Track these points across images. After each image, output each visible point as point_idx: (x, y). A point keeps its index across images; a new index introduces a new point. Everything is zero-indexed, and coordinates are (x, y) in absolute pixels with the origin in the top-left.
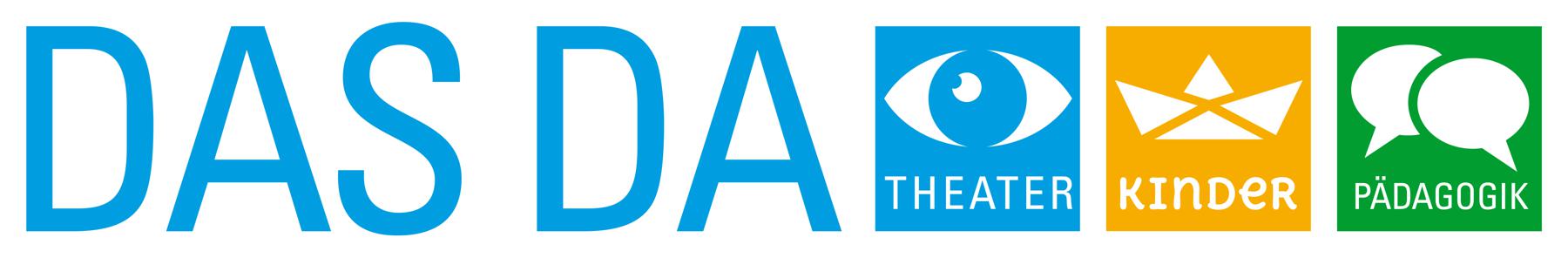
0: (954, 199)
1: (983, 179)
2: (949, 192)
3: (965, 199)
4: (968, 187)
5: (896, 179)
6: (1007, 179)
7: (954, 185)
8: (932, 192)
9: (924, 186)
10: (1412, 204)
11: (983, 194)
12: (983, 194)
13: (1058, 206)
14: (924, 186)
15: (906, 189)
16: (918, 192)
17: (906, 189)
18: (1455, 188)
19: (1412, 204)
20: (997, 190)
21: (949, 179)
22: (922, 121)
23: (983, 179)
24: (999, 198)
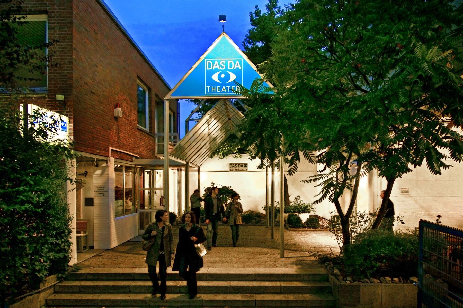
0: (219, 90)
1: (224, 87)
2: (218, 89)
3: (221, 90)
4: (442, 57)
5: (208, 87)
6: (228, 87)
7: (219, 88)
8: (215, 89)
9: (214, 88)
10: (234, 68)
11: (224, 89)
12: (224, 89)
13: (169, 286)
14: (214, 88)
15: (210, 89)
16: (212, 89)
17: (210, 89)
18: (424, 118)
19: (234, 68)
20: (227, 89)
21: (218, 87)
22: (441, 58)
23: (224, 87)
24: (227, 90)
